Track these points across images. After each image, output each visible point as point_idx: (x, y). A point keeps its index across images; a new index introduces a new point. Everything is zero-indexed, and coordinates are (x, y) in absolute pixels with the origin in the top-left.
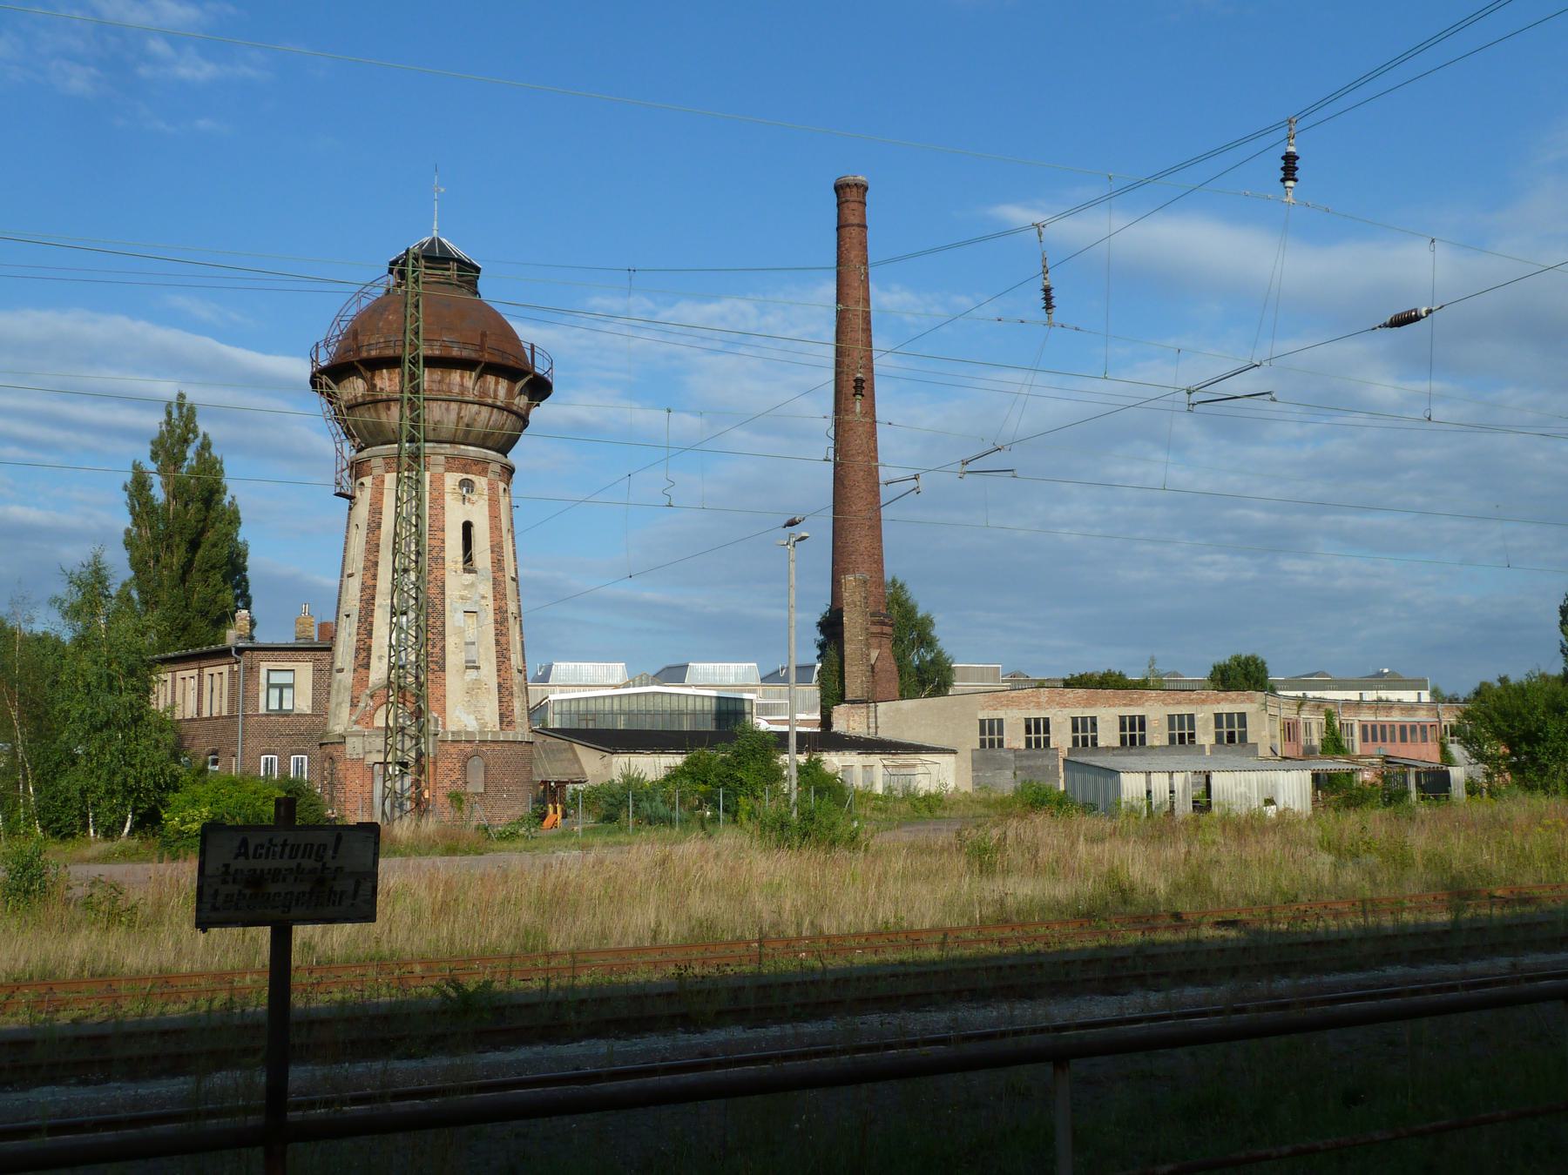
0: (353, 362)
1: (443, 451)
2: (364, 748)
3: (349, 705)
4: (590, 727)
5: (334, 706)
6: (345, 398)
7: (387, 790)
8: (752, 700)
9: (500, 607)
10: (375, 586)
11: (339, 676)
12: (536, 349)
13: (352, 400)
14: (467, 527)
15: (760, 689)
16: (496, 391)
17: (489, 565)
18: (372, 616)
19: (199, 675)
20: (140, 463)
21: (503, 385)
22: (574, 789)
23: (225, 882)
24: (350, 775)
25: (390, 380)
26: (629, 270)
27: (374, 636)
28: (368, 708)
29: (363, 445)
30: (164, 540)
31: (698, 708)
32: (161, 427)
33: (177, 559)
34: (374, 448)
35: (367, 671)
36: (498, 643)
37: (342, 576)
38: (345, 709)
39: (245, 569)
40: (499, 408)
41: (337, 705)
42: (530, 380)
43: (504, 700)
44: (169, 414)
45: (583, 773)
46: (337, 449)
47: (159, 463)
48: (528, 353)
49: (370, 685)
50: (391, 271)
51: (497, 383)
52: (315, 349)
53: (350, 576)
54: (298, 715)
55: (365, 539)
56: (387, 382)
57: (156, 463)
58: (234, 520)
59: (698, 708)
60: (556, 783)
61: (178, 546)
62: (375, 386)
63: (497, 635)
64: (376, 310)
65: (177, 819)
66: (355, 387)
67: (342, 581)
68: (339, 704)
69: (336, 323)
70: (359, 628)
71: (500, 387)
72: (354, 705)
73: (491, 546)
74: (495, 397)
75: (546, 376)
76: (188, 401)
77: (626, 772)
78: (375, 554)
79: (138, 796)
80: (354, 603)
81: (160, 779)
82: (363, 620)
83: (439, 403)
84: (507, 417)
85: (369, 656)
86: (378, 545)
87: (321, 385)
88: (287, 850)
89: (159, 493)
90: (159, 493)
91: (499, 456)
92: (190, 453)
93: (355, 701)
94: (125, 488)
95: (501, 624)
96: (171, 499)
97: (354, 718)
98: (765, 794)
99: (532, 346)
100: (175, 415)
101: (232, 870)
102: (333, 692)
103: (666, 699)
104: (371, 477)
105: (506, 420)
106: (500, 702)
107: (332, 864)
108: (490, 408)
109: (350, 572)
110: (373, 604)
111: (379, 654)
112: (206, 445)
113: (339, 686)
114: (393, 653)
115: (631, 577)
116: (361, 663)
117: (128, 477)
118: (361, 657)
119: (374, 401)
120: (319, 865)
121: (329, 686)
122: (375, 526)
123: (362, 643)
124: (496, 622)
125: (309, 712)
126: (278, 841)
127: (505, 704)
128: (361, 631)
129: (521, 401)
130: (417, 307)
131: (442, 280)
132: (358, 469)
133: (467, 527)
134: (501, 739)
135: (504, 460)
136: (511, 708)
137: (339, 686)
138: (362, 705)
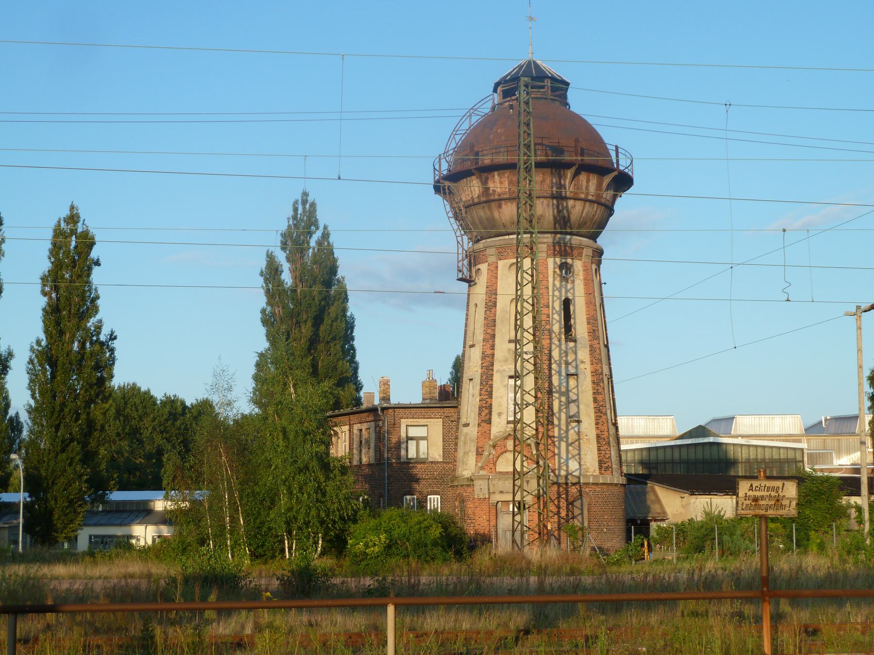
0: (471, 170)
1: (545, 240)
2: (489, 489)
3: (475, 454)
4: (782, 457)
5: (462, 454)
6: (464, 199)
7: (516, 524)
8: (802, 450)
9: (596, 370)
10: (493, 355)
11: (465, 430)
12: (620, 150)
13: (469, 200)
14: (567, 304)
15: (804, 439)
16: (587, 187)
17: (586, 335)
18: (492, 380)
19: (350, 430)
20: (272, 253)
21: (594, 180)
22: (659, 526)
23: (746, 500)
24: (478, 511)
25: (501, 183)
26: (726, 105)
27: (494, 396)
28: (491, 456)
29: (479, 238)
30: (294, 318)
31: (752, 457)
32: (289, 222)
33: (306, 330)
34: (488, 240)
35: (488, 425)
36: (595, 400)
37: (464, 347)
38: (472, 459)
39: (353, 339)
40: (591, 201)
41: (464, 454)
42: (615, 177)
43: (602, 448)
44: (296, 210)
45: (664, 513)
46: (458, 242)
47: (288, 252)
48: (613, 154)
49: (492, 437)
50: (495, 91)
51: (588, 181)
52: (438, 159)
53: (472, 346)
54: (432, 462)
55: (484, 316)
56: (499, 184)
57: (285, 252)
58: (343, 297)
59: (752, 457)
60: (641, 520)
61: (306, 322)
62: (488, 189)
63: (594, 393)
64: (487, 124)
65: (361, 544)
66: (472, 188)
67: (464, 351)
68: (466, 453)
69: (452, 136)
70: (481, 389)
71: (591, 184)
72: (479, 454)
73: (588, 319)
74: (587, 194)
75: (626, 170)
76: (310, 199)
77: (708, 510)
78: (493, 328)
79: (328, 526)
80: (476, 369)
81: (344, 513)
82: (484, 383)
83: (541, 200)
84: (597, 209)
85: (490, 413)
86: (494, 321)
87: (444, 189)
88: (766, 488)
89: (287, 277)
90: (287, 277)
91: (590, 242)
92: (313, 242)
93: (480, 450)
94: (262, 274)
95: (598, 384)
96: (298, 283)
97: (480, 464)
98: (832, 529)
99: (617, 147)
100: (300, 211)
101: (748, 495)
102: (461, 443)
103: (692, 450)
104: (487, 264)
105: (596, 211)
106: (599, 450)
107: (781, 494)
108: (583, 202)
109: (471, 343)
110: (492, 370)
111: (498, 411)
112: (326, 236)
113: (465, 438)
114: (517, 410)
115: (735, 348)
116: (484, 419)
117: (263, 264)
118: (483, 414)
119: (488, 200)
120: (777, 494)
121: (457, 438)
122: (491, 305)
123: (484, 402)
124: (593, 382)
125: (441, 460)
126: (763, 485)
127: (603, 452)
128: (483, 392)
129: (608, 195)
130: (528, 125)
131: (539, 96)
132: (473, 259)
133: (567, 304)
134: (601, 482)
135: (595, 246)
136: (609, 455)
137: (465, 438)
138: (486, 453)
